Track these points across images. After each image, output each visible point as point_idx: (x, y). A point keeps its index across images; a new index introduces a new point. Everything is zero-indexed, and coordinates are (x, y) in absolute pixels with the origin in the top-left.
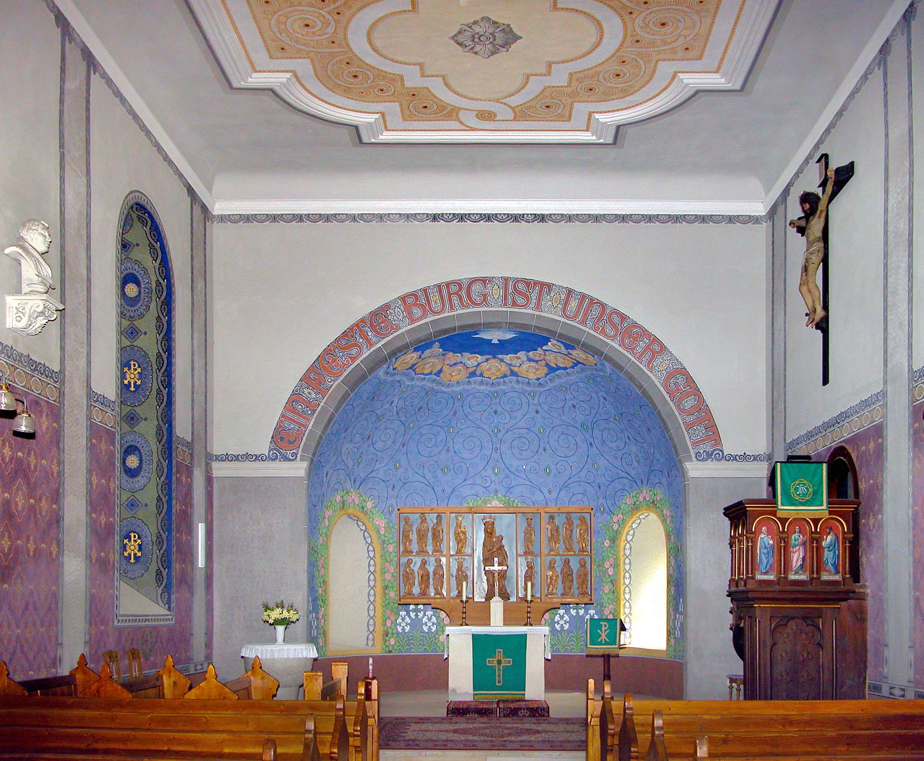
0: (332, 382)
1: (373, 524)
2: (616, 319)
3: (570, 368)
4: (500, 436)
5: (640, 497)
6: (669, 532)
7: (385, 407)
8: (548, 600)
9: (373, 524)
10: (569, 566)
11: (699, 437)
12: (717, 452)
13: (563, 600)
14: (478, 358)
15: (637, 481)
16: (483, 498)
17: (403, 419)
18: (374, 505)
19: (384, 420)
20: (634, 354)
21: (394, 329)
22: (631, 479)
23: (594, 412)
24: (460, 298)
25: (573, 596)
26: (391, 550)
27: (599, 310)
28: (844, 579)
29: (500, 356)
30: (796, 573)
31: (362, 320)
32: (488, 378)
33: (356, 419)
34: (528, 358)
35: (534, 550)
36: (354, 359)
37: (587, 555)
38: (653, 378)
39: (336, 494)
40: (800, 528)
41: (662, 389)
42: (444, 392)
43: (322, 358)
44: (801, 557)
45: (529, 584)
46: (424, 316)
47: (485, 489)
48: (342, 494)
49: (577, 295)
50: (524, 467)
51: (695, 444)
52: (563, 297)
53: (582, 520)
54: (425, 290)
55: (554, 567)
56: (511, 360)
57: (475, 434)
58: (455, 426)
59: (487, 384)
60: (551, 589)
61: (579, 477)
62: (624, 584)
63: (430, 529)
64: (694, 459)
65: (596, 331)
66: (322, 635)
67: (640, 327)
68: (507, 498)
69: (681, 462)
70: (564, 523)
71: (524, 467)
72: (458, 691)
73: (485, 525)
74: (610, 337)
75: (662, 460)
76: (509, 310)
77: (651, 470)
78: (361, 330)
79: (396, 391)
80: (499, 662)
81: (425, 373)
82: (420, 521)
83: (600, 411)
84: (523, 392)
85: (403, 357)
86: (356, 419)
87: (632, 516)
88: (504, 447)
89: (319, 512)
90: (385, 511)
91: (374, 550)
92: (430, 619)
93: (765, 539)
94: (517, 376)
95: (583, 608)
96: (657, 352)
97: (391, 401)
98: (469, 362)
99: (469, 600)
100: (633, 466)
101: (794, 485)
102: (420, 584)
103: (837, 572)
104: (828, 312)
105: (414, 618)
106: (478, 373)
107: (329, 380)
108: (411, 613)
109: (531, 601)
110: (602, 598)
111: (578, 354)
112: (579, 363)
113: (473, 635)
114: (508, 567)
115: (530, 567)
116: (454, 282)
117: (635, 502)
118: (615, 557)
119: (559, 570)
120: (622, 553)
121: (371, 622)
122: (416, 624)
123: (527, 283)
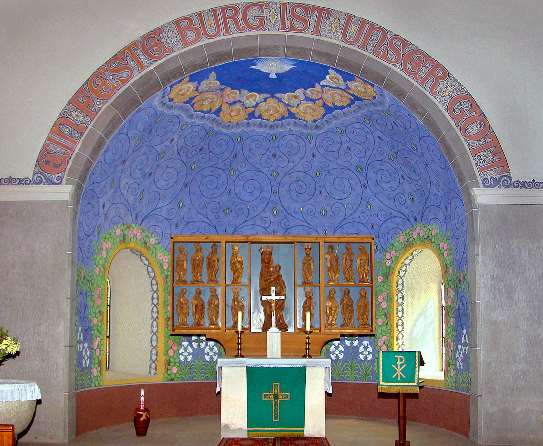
0: (102, 105)
3: (347, 106)
4: (279, 179)
5: (414, 233)
6: (446, 265)
7: (164, 144)
8: (327, 331)
10: (349, 297)
12: (505, 178)
13: (343, 331)
14: (256, 96)
15: (410, 219)
17: (185, 159)
18: (157, 242)
19: (165, 158)
20: (416, 79)
22: (404, 217)
23: (369, 153)
24: (236, 21)
25: (353, 327)
29: (278, 95)
31: (135, 44)
32: (267, 120)
33: (134, 152)
34: (305, 97)
35: (313, 281)
36: (124, 82)
37: (368, 286)
38: (437, 103)
39: (116, 227)
42: (225, 134)
43: (91, 81)
45: (308, 314)
46: (198, 39)
48: (122, 228)
50: (301, 209)
51: (482, 170)
52: (342, 22)
53: (362, 250)
54: (200, 15)
55: (333, 298)
56: (289, 99)
57: (255, 177)
58: (236, 169)
59: (266, 127)
60: (330, 320)
62: (397, 316)
63: (205, 258)
64: (481, 185)
66: (97, 365)
67: (423, 53)
69: (467, 190)
70: (343, 254)
71: (301, 209)
72: (232, 427)
73: (262, 254)
74: (392, 62)
75: (440, 194)
77: (426, 206)
78: (132, 53)
79: (176, 127)
80: (276, 397)
81: (205, 110)
82: (195, 250)
83: (375, 152)
84: (300, 136)
85: (179, 86)
86: (134, 152)
87: (405, 252)
88: (283, 191)
89: (94, 243)
91: (157, 284)
92: (211, 349)
94: (295, 118)
95: (357, 339)
96: (441, 78)
97: (171, 138)
98: (247, 101)
99: (246, 331)
100: (406, 205)
102: (195, 314)
105: (196, 348)
107: (98, 103)
108: (193, 343)
109: (311, 332)
111: (357, 86)
112: (357, 98)
113: (247, 367)
114: (285, 297)
115: (309, 298)
116: (229, 7)
117: (408, 239)
118: (388, 291)
119: (338, 300)
120: (395, 288)
121: (154, 352)
122: (198, 354)
123: (306, 8)
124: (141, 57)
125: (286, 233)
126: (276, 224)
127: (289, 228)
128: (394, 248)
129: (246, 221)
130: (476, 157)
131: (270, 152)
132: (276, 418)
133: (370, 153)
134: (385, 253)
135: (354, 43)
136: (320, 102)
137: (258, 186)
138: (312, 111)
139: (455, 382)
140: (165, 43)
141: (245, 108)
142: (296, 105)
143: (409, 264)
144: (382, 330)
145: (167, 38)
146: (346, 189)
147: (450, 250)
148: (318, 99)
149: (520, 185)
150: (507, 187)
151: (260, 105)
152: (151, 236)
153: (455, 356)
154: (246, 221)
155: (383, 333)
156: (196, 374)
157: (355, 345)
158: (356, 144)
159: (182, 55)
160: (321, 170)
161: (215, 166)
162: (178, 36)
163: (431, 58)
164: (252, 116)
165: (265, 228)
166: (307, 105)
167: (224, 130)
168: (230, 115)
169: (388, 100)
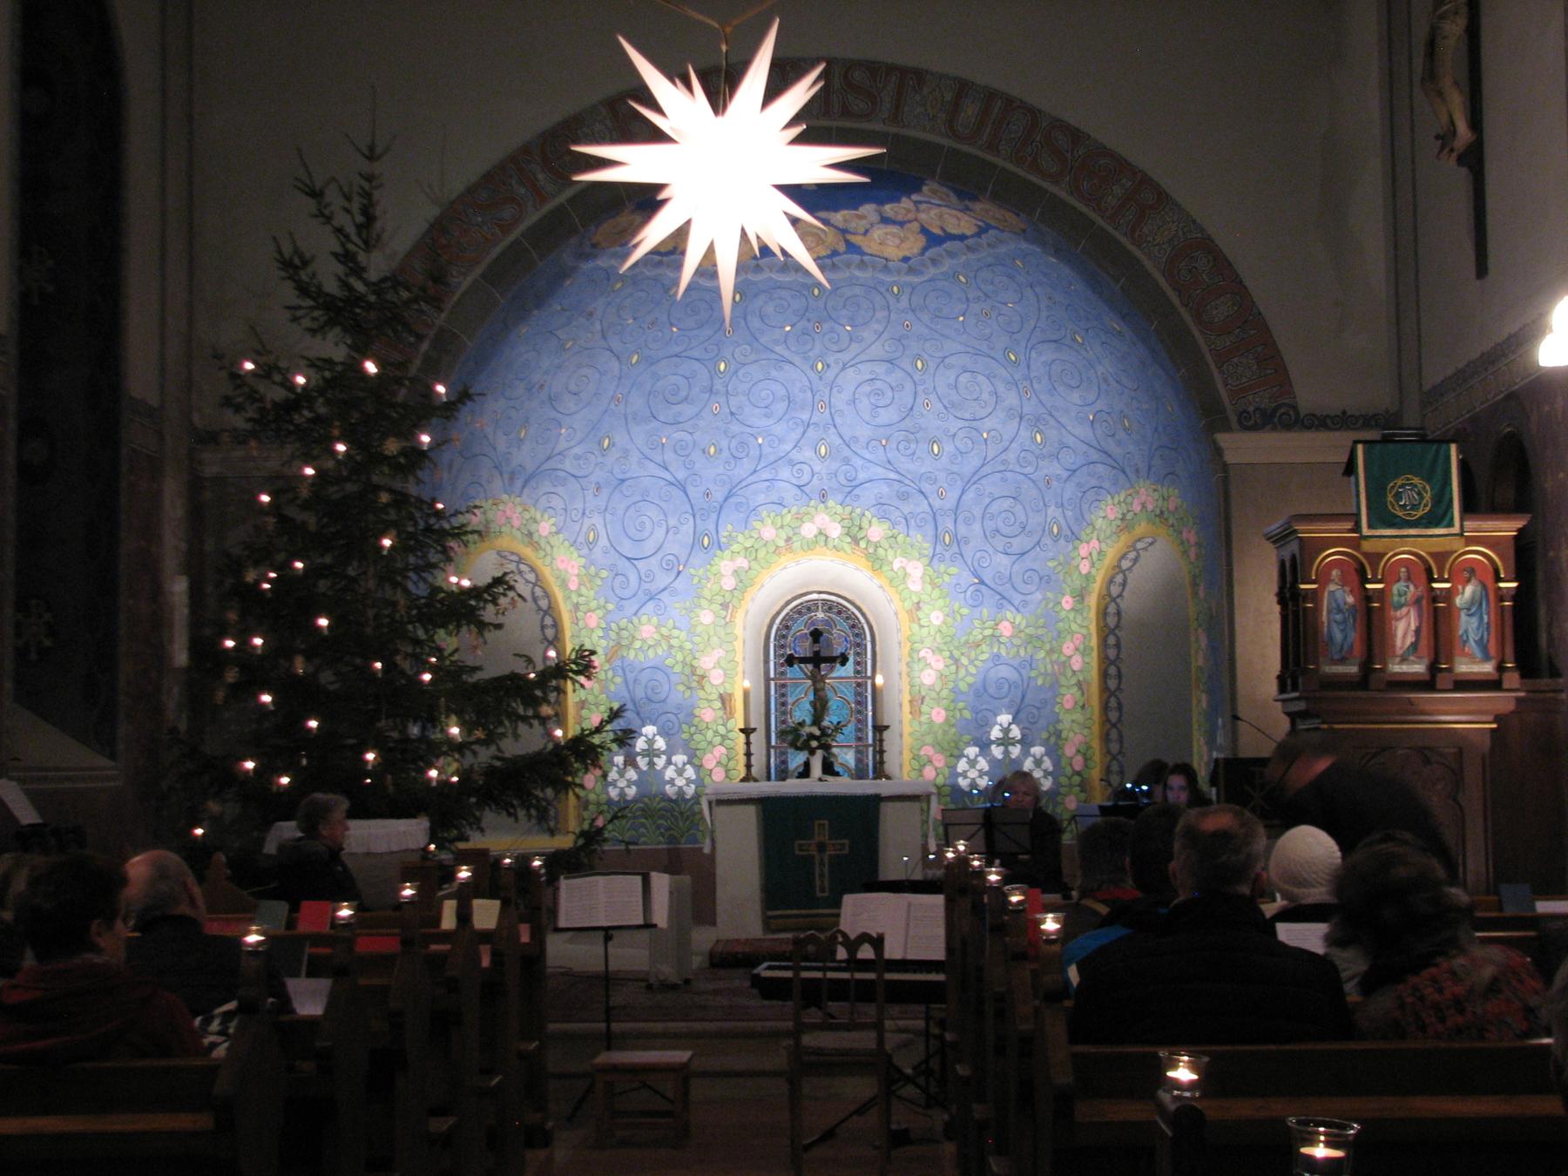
1: (553, 570)
4: (830, 375)
9: (553, 570)
11: (1244, 380)
16: (794, 510)
18: (554, 529)
26: (593, 624)
28: (1500, 668)
30: (1404, 660)
31: (526, 149)
36: (506, 230)
40: (1408, 571)
41: (1162, 281)
44: (1413, 627)
47: (799, 492)
50: (884, 442)
52: (948, 96)
58: (730, 357)
61: (1004, 462)
64: (1234, 424)
67: (1111, 154)
68: (848, 509)
76: (834, 124)
90: (581, 539)
92: (680, 772)
93: (1339, 594)
101: (1393, 487)
103: (1487, 658)
104: (1481, 132)
108: (639, 758)
123: (872, 68)
124: (541, 176)
125: (848, 498)
128: (1095, 533)
129: (755, 471)
132: (822, 890)
136: (916, 226)
137: (783, 392)
142: (863, 230)
143: (1129, 569)
146: (985, 396)
149: (1316, 423)
150: (1288, 427)
152: (542, 516)
154: (755, 471)
156: (646, 828)
157: (1013, 756)
165: (799, 487)
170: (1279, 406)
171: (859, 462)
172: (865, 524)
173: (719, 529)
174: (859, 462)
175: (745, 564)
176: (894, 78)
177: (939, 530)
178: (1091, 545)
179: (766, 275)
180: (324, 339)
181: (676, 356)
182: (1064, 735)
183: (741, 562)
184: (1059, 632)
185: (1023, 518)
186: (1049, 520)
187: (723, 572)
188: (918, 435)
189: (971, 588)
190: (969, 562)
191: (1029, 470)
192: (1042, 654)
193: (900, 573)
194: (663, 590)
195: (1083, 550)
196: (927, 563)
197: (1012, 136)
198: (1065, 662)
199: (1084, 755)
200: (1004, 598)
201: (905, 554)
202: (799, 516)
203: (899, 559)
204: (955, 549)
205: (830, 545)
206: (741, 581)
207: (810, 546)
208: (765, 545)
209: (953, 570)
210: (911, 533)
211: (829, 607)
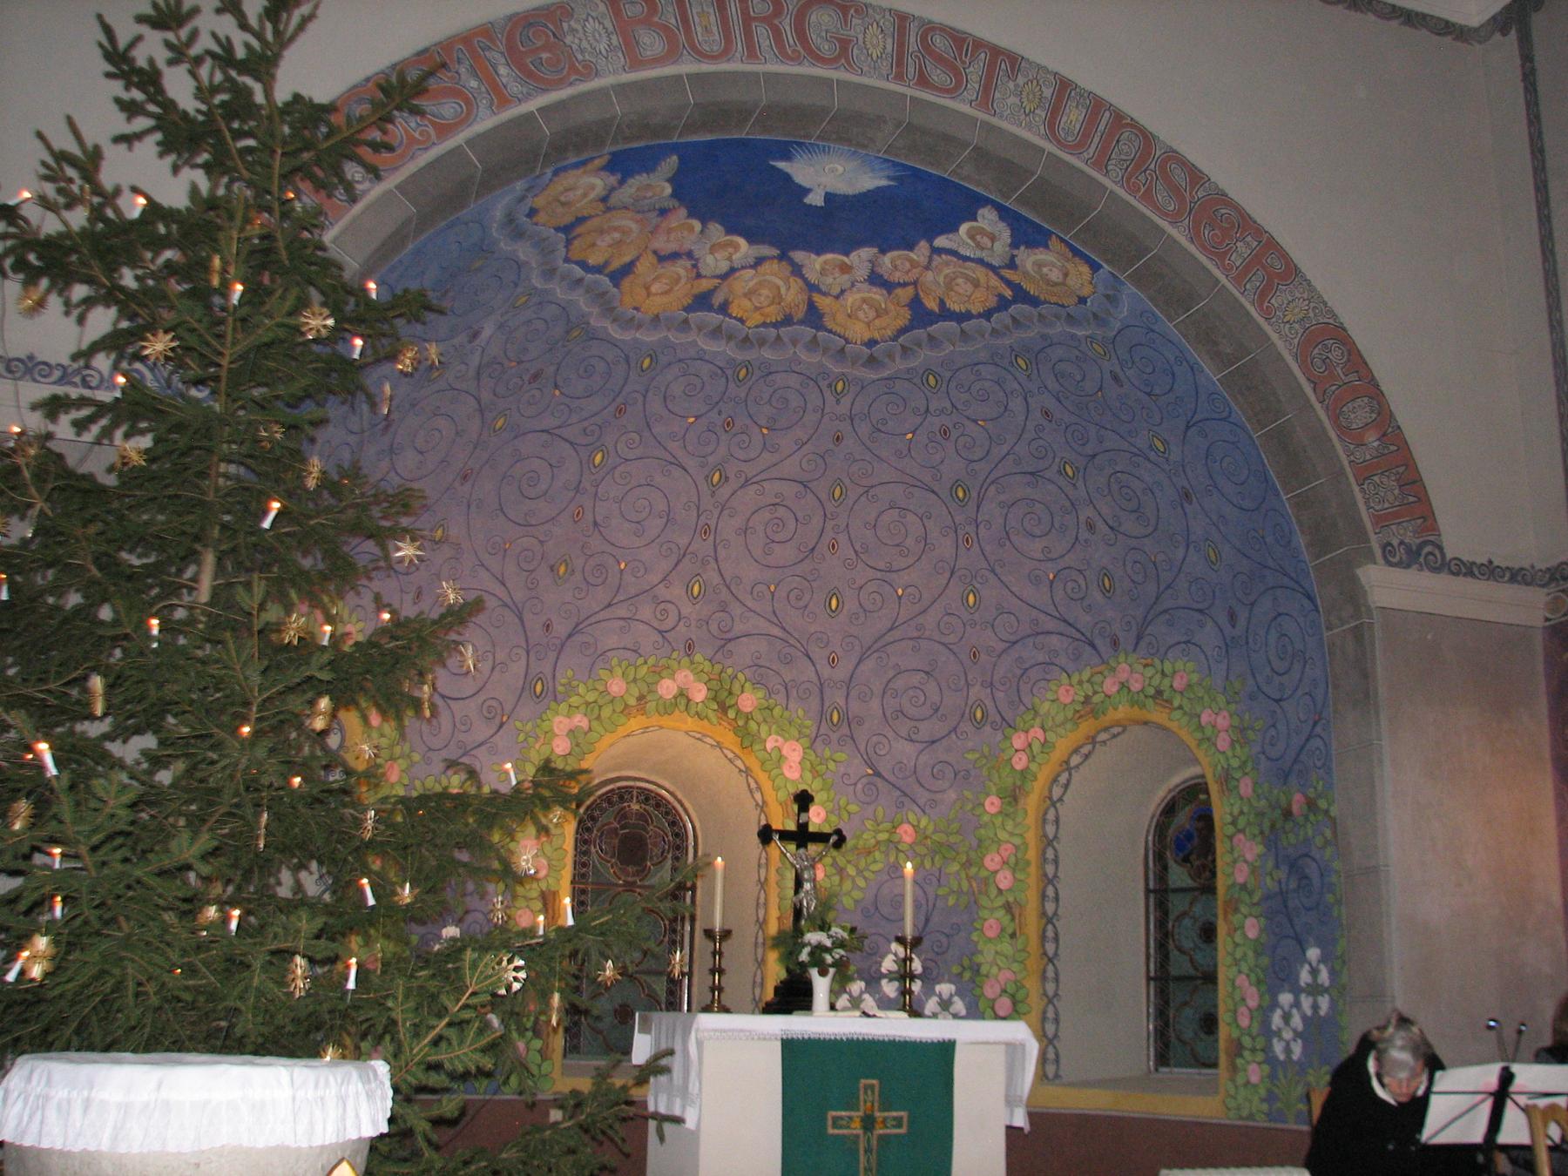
2: (1180, 177)
4: (725, 491)
7: (456, 341)
12: (1428, 549)
14: (737, 247)
15: (1098, 642)
16: (651, 661)
17: (486, 396)
20: (1226, 270)
21: (577, 72)
24: (777, 34)
27: (1136, 144)
31: (485, 31)
34: (873, 271)
38: (1274, 337)
42: (614, 344)
46: (672, 55)
47: (660, 639)
49: (1081, 96)
50: (772, 588)
51: (1381, 521)
52: (1048, 92)
59: (730, 338)
65: (1133, 190)
68: (718, 668)
81: (591, 262)
94: (819, 326)
98: (710, 259)
106: (717, 300)
110: (976, 952)
118: (1017, 841)
123: (959, 39)
124: (503, 70)
125: (720, 653)
126: (693, 623)
127: (730, 640)
128: (1038, 721)
129: (609, 605)
130: (1365, 487)
131: (720, 413)
133: (1005, 448)
134: (1009, 731)
135: (1078, 147)
136: (905, 294)
137: (661, 506)
138: (872, 314)
139: (1270, 1098)
140: (575, 47)
141: (694, 275)
144: (997, 953)
145: (581, 35)
146: (910, 542)
147: (1242, 730)
148: (905, 285)
149: (1464, 570)
150: (1436, 570)
151: (737, 274)
153: (1266, 1023)
154: (609, 605)
155: (1001, 961)
158: (967, 423)
159: (622, 89)
160: (847, 481)
161: (556, 431)
162: (614, 37)
163: (1255, 222)
164: (702, 301)
166: (866, 295)
167: (615, 332)
168: (647, 288)
169: (1124, 311)
170: (1426, 543)
171: (737, 610)
172: (736, 688)
173: (558, 675)
174: (737, 610)
175: (585, 724)
176: (983, 55)
177: (827, 704)
178: (1032, 733)
179: (692, 336)
180: (176, 169)
181: (546, 431)
182: (984, 970)
183: (580, 720)
184: (980, 841)
185: (936, 698)
186: (970, 703)
187: (556, 730)
188: (814, 584)
189: (864, 780)
190: (862, 748)
191: (951, 639)
192: (954, 867)
193: (775, 755)
194: (479, 746)
195: (1018, 741)
196: (807, 745)
197: (1123, 157)
198: (986, 879)
199: (1013, 996)
200: (906, 795)
201: (782, 732)
202: (658, 669)
203: (774, 736)
204: (845, 730)
205: (692, 712)
206: (578, 745)
207: (667, 708)
208: (612, 701)
209: (840, 756)
210: (791, 705)
211: (647, 797)
